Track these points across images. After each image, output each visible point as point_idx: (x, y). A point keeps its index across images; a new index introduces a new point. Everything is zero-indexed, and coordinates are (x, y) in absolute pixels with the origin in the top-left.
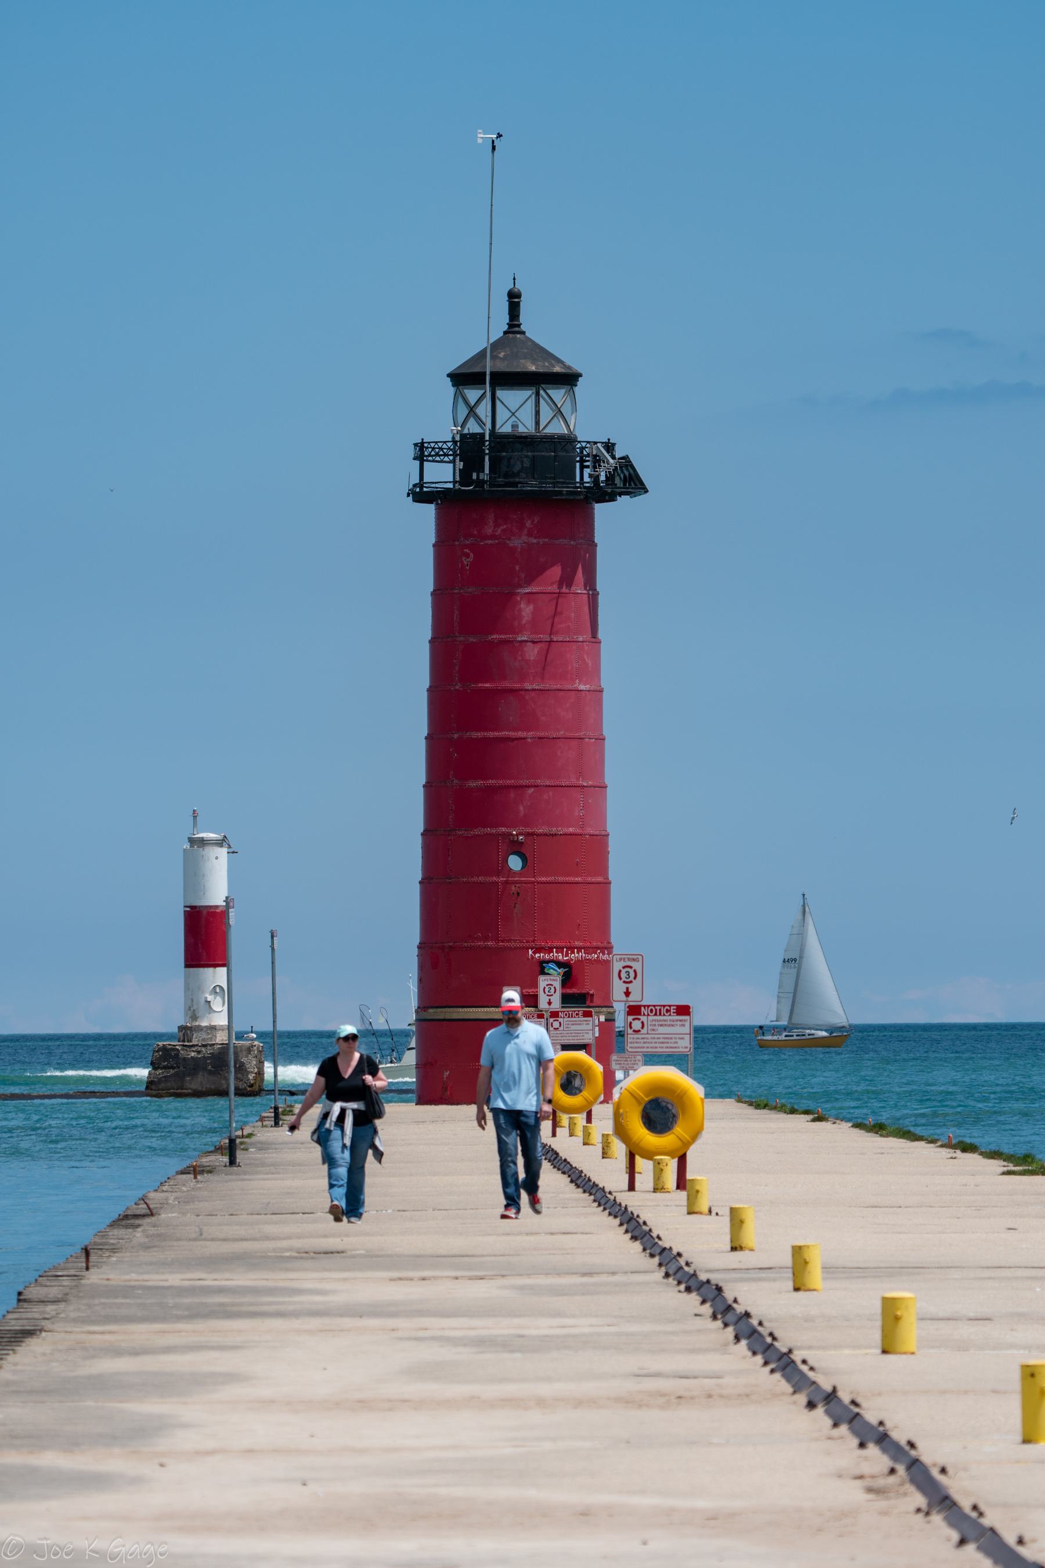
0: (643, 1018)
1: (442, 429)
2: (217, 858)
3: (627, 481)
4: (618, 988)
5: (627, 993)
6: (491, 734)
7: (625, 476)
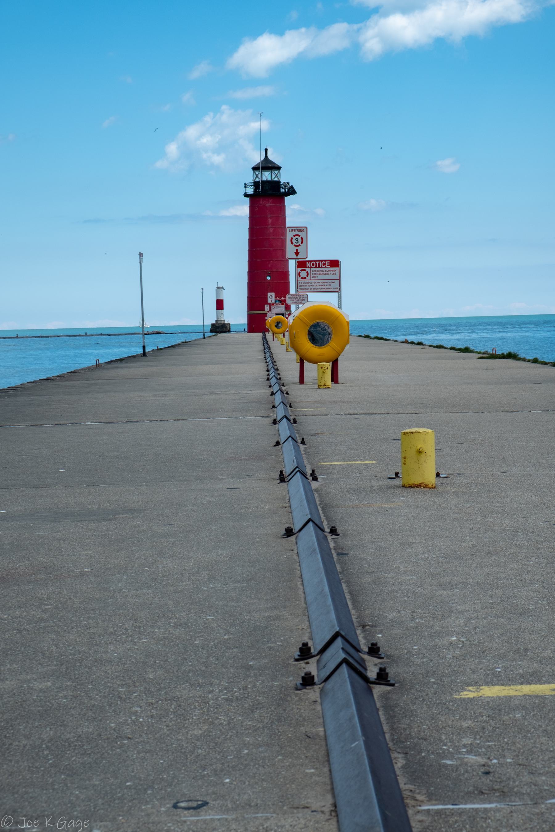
0: (308, 270)
3: (292, 191)
4: (290, 250)
5: (297, 253)
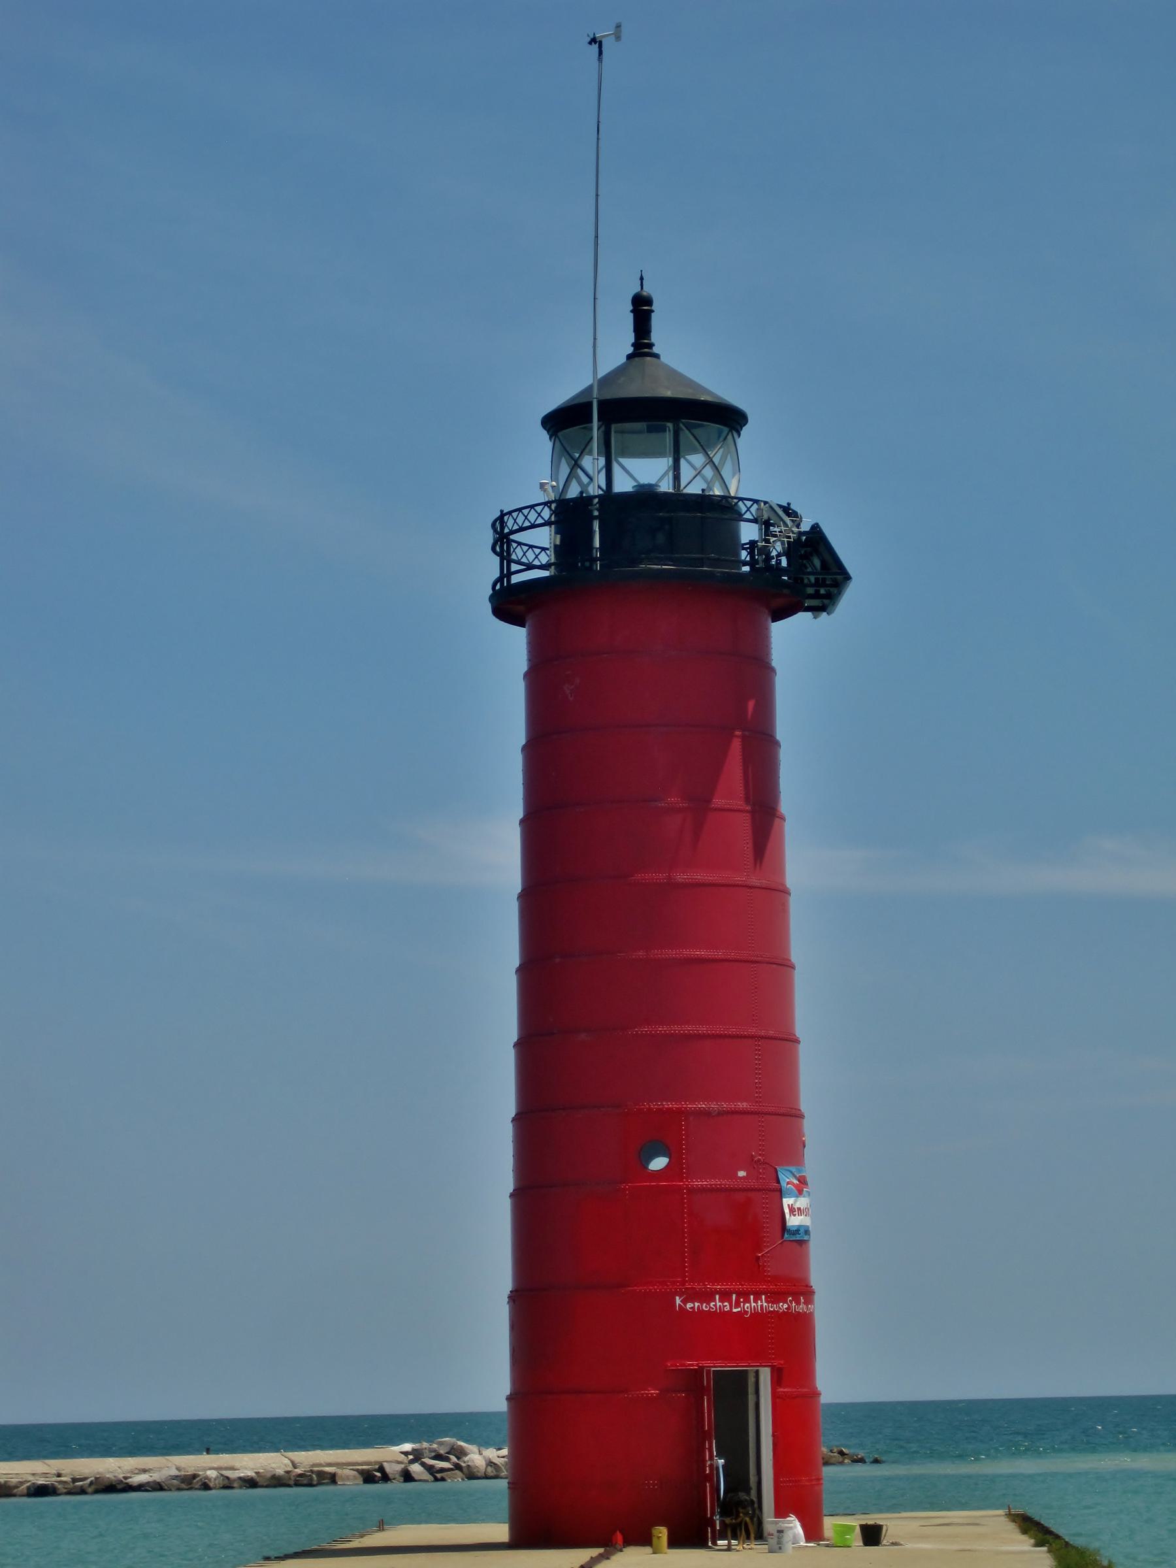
3: (810, 574)
6: (676, 1029)
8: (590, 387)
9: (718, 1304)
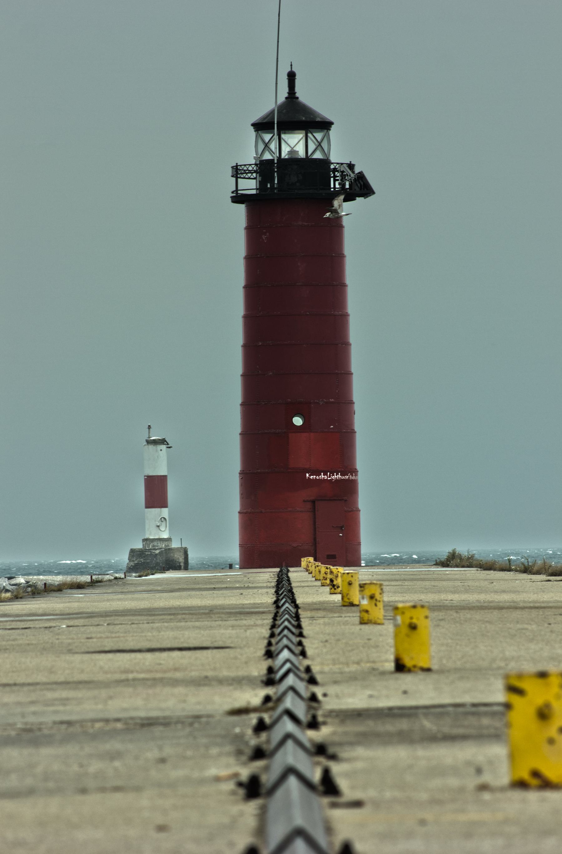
1: (249, 157)
2: (161, 450)
3: (360, 188)
7: (361, 185)
8: (272, 112)
9: (323, 476)
